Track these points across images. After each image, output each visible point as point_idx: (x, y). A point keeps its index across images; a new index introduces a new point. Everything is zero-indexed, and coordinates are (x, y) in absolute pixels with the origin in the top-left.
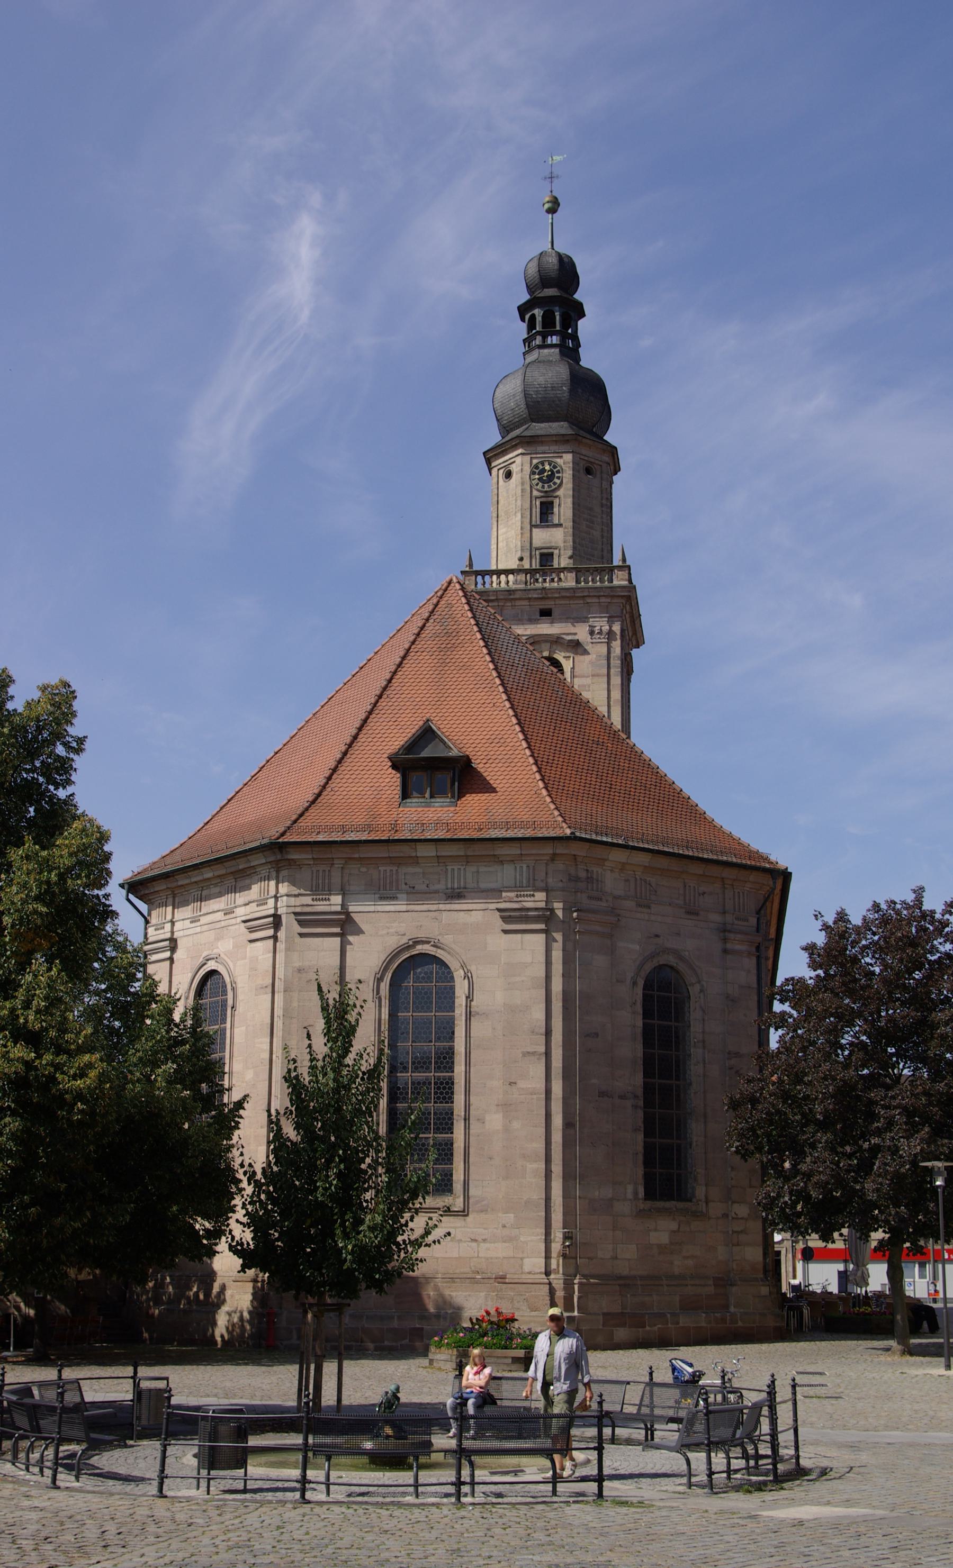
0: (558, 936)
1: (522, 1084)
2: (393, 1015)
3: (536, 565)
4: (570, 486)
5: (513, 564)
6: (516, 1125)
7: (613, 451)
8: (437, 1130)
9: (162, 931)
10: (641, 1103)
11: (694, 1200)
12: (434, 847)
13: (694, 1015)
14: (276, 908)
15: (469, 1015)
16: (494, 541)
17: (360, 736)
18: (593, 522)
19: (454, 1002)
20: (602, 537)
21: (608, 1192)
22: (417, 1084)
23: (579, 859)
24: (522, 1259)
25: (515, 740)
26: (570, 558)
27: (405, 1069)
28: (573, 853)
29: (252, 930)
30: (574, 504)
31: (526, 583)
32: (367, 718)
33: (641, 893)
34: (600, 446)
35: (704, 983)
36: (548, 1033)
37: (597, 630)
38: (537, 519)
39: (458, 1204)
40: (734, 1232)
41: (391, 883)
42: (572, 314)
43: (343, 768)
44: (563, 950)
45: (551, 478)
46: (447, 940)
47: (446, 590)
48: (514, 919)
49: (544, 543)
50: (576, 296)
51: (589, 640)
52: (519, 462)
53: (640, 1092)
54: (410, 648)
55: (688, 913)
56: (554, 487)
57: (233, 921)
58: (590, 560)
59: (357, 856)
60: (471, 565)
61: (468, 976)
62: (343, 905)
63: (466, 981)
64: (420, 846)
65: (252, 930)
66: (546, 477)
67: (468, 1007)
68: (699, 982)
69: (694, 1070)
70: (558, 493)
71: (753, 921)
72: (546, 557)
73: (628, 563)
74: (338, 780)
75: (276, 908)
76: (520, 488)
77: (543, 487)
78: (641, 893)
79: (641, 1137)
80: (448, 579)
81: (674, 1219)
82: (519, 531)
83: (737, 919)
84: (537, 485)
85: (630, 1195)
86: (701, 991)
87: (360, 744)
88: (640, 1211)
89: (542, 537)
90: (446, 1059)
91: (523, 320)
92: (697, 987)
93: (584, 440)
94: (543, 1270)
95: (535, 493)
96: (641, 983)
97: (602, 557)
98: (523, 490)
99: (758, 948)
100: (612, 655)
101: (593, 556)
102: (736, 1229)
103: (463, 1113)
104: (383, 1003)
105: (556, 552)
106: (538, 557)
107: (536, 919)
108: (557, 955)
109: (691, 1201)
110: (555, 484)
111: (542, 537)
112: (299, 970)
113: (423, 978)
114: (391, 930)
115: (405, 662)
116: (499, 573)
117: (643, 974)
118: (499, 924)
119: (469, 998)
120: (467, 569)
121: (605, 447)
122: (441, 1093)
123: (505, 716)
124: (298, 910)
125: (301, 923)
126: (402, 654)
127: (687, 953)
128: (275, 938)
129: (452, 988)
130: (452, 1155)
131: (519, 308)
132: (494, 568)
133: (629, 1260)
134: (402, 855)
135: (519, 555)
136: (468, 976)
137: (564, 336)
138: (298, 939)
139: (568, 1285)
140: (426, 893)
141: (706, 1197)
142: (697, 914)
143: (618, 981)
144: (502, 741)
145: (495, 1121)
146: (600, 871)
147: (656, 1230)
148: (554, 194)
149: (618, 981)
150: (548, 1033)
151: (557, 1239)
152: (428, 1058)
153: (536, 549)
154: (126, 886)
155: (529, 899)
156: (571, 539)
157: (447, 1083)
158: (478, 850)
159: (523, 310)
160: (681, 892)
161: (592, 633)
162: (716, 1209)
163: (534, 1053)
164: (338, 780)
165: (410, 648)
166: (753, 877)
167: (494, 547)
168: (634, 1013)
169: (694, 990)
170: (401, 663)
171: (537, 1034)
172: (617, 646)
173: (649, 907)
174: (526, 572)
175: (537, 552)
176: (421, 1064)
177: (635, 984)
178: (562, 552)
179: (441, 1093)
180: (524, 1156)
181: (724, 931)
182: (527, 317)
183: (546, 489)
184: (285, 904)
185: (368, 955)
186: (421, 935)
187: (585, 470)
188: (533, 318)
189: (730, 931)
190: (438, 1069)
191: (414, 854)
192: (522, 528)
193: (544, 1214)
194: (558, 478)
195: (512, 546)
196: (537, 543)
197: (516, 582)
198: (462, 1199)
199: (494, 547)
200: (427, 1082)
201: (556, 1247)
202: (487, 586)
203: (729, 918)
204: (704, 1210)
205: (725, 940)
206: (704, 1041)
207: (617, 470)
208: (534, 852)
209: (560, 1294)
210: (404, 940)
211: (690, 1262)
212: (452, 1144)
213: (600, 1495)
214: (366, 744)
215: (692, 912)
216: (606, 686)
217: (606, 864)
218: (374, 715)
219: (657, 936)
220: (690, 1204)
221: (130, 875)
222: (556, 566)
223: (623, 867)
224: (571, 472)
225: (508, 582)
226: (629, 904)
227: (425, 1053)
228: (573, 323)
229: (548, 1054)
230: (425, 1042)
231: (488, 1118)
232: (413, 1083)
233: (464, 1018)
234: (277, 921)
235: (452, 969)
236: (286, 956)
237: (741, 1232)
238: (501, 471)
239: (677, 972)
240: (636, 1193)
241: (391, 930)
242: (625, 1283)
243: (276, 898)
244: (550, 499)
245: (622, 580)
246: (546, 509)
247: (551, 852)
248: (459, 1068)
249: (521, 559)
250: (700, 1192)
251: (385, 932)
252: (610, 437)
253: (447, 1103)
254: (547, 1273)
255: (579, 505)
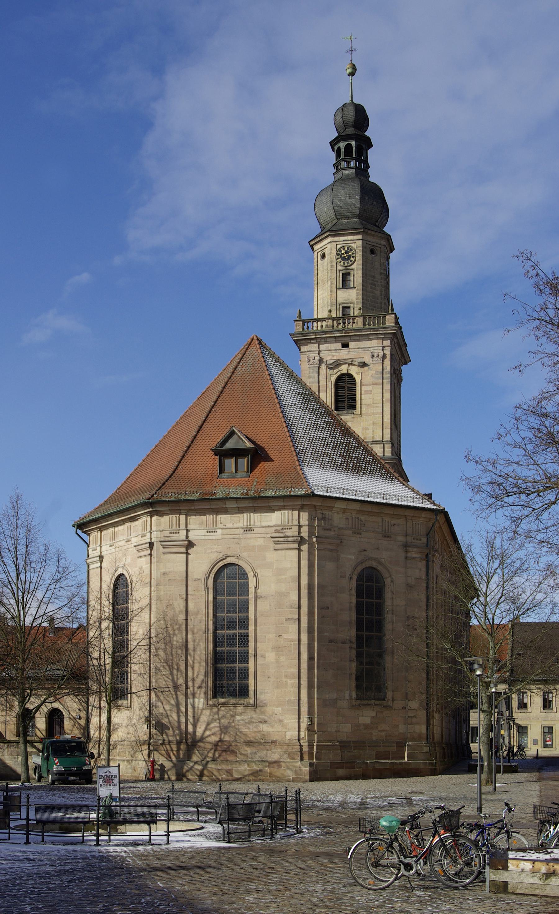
0: (305, 547)
1: (285, 636)
2: (215, 598)
3: (339, 314)
4: (361, 262)
5: (325, 315)
6: (282, 659)
7: (388, 238)
8: (240, 662)
9: (95, 551)
10: (354, 646)
11: (386, 699)
12: (235, 502)
13: (388, 595)
14: (151, 539)
15: (256, 598)
16: (315, 299)
17: (198, 436)
18: (375, 285)
19: (248, 591)
20: (381, 294)
21: (335, 696)
22: (229, 636)
23: (317, 507)
24: (285, 732)
25: (284, 436)
26: (360, 309)
27: (222, 628)
28: (313, 503)
29: (139, 551)
30: (362, 274)
31: (333, 326)
32: (202, 425)
33: (355, 526)
34: (380, 235)
35: (394, 578)
36: (299, 607)
37: (376, 355)
38: (340, 284)
39: (252, 701)
40: (409, 717)
41: (213, 523)
42: (364, 146)
43: (188, 456)
44: (308, 560)
45: (349, 257)
46: (245, 554)
47: (250, 344)
48: (280, 540)
49: (345, 300)
50: (365, 134)
51: (371, 362)
52: (329, 245)
53: (354, 640)
54: (228, 381)
55: (385, 536)
56: (350, 263)
57: (130, 546)
58: (373, 310)
59: (193, 508)
60: (300, 316)
61: (256, 576)
62: (187, 536)
63: (255, 578)
64: (227, 502)
65: (139, 551)
66: (345, 256)
67: (256, 593)
68: (390, 576)
69: (388, 627)
70: (352, 267)
71: (424, 540)
72: (346, 308)
73: (395, 312)
74: (185, 463)
75: (151, 539)
76: (330, 265)
77: (344, 263)
78: (355, 526)
79: (354, 665)
80: (251, 337)
81: (373, 710)
82: (330, 293)
83: (415, 539)
84: (340, 262)
85: (347, 697)
86: (392, 581)
87: (197, 441)
88: (353, 706)
89: (345, 296)
90: (244, 623)
91: (333, 151)
92: (389, 580)
93: (370, 232)
94: (297, 738)
95: (339, 268)
96: (355, 577)
97: (381, 308)
98: (332, 266)
99: (427, 556)
100: (384, 371)
101: (375, 307)
102: (410, 715)
103: (254, 653)
104: (209, 592)
105: (352, 305)
106: (341, 309)
107: (293, 542)
108: (304, 563)
109: (384, 700)
110: (351, 261)
111: (345, 296)
112: (164, 574)
113: (232, 577)
114: (213, 550)
115: (225, 390)
116: (318, 320)
117: (356, 572)
118: (272, 545)
119: (256, 587)
120: (298, 319)
121: (382, 235)
122: (242, 641)
123: (280, 422)
124: (163, 539)
125: (164, 547)
126: (223, 385)
127: (383, 560)
128: (151, 555)
129: (248, 583)
130: (248, 676)
131: (330, 143)
132: (315, 317)
133: (347, 732)
134: (218, 507)
135: (329, 308)
136: (256, 576)
137: (358, 159)
138: (162, 556)
139: (310, 746)
140: (232, 528)
141: (393, 698)
142: (390, 537)
143: (341, 577)
144: (277, 437)
145: (271, 657)
146: (330, 513)
147: (363, 716)
148: (353, 62)
149: (341, 577)
150: (299, 607)
151: (305, 721)
152: (235, 622)
153: (340, 304)
154: (76, 526)
155: (288, 530)
156: (361, 296)
157: (245, 636)
158: (260, 503)
159: (333, 144)
160: (381, 524)
161: (373, 357)
162: (399, 704)
163: (292, 619)
164: (185, 463)
165: (228, 381)
166: (424, 515)
167: (315, 303)
168: (350, 595)
169: (388, 581)
170: (222, 391)
171: (294, 608)
172: (387, 362)
173: (360, 534)
174: (334, 319)
175: (341, 307)
176: (231, 625)
177: (351, 578)
178: (355, 305)
179: (242, 641)
180: (286, 676)
181: (406, 546)
182: (336, 148)
183: (346, 265)
184: (155, 536)
185: (202, 564)
186: (230, 553)
187: (370, 251)
188: (339, 148)
189: (409, 547)
190: (240, 628)
191: (224, 506)
192: (331, 291)
193: (297, 707)
194: (353, 257)
195: (326, 302)
196: (340, 300)
197: (327, 326)
198: (253, 699)
199: (315, 303)
200: (234, 636)
201: (304, 726)
202: (310, 329)
203: (409, 539)
204: (391, 705)
205: (406, 552)
206: (393, 610)
207: (392, 249)
208: (291, 503)
209: (305, 749)
210: (220, 556)
211: (383, 734)
212: (248, 670)
213: (43, 841)
214: (201, 441)
215: (386, 536)
216: (381, 391)
217: (334, 509)
218: (206, 423)
219: (365, 550)
220: (383, 702)
221: (78, 519)
222: (352, 315)
223: (344, 511)
224: (361, 253)
225: (322, 326)
226: (349, 532)
227: (233, 619)
228: (364, 152)
229: (299, 619)
230: (233, 613)
231: (267, 655)
232: (227, 636)
233: (254, 599)
234: (151, 545)
235: (247, 572)
236: (157, 565)
237: (414, 717)
238: (319, 254)
239: (378, 571)
240: (351, 696)
241: (213, 550)
242: (344, 745)
243: (151, 533)
244: (348, 271)
245: (391, 322)
246: (346, 276)
247: (300, 503)
248: (251, 628)
249: (330, 311)
250: (389, 695)
251: (210, 551)
252: (386, 229)
253: (245, 647)
254: (299, 740)
255: (366, 274)
